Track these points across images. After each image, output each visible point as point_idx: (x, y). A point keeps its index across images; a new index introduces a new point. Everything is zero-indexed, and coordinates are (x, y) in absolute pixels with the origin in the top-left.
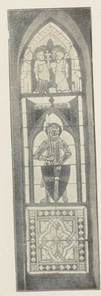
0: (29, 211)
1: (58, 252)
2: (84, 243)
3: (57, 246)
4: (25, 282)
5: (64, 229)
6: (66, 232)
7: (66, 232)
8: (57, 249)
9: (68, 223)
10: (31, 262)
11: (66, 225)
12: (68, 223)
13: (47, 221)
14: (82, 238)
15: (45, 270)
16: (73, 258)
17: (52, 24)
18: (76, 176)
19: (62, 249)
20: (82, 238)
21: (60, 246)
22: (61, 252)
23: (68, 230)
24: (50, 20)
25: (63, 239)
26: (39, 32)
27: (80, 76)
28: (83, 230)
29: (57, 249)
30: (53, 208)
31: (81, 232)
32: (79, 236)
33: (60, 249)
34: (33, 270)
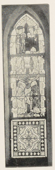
0: (13, 121)
1: (29, 145)
2: (44, 139)
3: (28, 143)
4: (11, 162)
5: (33, 132)
6: (24, 143)
7: (24, 143)
8: (29, 143)
9: (23, 148)
10: (14, 151)
11: (34, 130)
12: (23, 148)
13: (34, 149)
14: (42, 137)
15: (22, 155)
16: (37, 149)
17: (27, 14)
18: (51, 66)
19: (26, 133)
20: (42, 137)
21: (31, 142)
22: (31, 145)
23: (21, 147)
24: (26, 12)
25: (26, 140)
26: (20, 19)
27: (44, 44)
28: (43, 132)
29: (29, 143)
30: (27, 120)
31: (42, 134)
32: (41, 136)
33: (27, 133)
34: (15, 156)
